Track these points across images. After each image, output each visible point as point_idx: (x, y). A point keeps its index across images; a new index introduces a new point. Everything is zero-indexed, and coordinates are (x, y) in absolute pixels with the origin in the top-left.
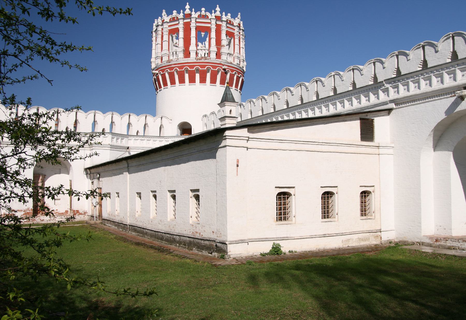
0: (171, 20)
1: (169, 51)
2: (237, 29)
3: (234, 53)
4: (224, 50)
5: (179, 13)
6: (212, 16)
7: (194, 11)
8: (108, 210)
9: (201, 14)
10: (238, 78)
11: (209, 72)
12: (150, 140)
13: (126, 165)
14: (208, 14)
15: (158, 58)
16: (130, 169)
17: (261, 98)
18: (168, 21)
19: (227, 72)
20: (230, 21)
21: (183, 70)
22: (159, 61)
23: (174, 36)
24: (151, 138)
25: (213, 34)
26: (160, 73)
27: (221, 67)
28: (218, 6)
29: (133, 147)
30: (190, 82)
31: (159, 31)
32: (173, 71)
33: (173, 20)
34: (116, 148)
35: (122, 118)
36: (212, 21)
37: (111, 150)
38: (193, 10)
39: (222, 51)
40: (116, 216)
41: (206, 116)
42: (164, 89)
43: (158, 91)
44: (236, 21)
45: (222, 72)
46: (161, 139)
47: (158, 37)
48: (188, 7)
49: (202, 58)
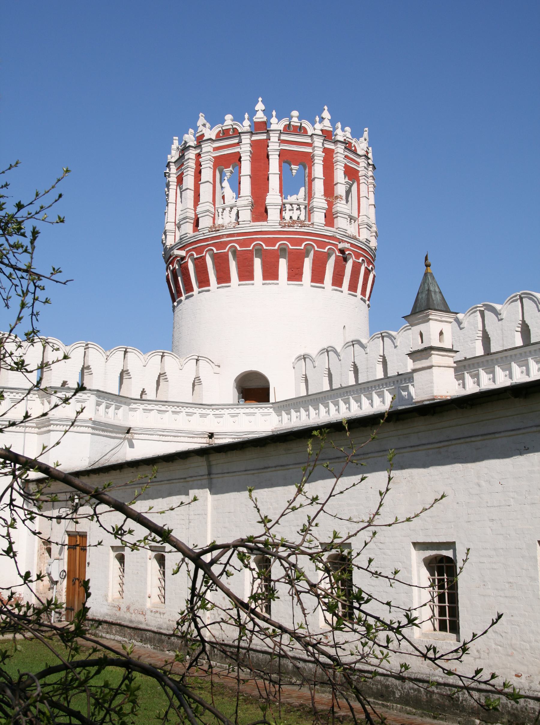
0: (221, 135)
1: (214, 205)
2: (363, 162)
3: (359, 216)
4: (340, 206)
5: (239, 119)
6: (315, 129)
7: (276, 117)
8: (110, 595)
9: (290, 123)
10: (367, 272)
11: (308, 257)
12: (179, 412)
13: (204, 470)
14: (306, 124)
15: (188, 220)
16: (214, 481)
17: (482, 309)
18: (214, 138)
19: (348, 256)
20: (350, 143)
21: (251, 248)
22: (188, 228)
23: (227, 171)
24: (183, 407)
25: (318, 170)
26: (193, 255)
27: (336, 246)
28: (326, 108)
29: (141, 429)
30: (265, 277)
31: (190, 160)
32: (226, 250)
33: (224, 135)
34: (103, 431)
35: (108, 356)
36: (315, 139)
37: (92, 434)
38: (274, 113)
39: (339, 209)
40: (149, 613)
41: (305, 359)
42: (199, 292)
43: (183, 298)
44: (361, 146)
45: (337, 257)
46: (204, 411)
47: (189, 173)
48: (260, 106)
49: (294, 222)
